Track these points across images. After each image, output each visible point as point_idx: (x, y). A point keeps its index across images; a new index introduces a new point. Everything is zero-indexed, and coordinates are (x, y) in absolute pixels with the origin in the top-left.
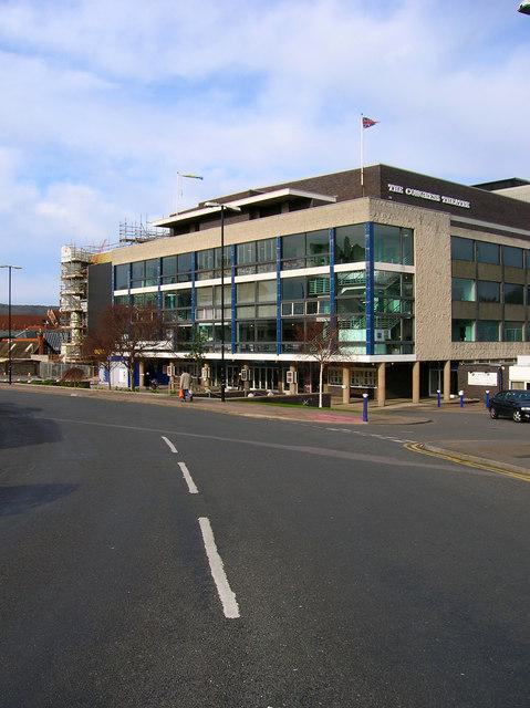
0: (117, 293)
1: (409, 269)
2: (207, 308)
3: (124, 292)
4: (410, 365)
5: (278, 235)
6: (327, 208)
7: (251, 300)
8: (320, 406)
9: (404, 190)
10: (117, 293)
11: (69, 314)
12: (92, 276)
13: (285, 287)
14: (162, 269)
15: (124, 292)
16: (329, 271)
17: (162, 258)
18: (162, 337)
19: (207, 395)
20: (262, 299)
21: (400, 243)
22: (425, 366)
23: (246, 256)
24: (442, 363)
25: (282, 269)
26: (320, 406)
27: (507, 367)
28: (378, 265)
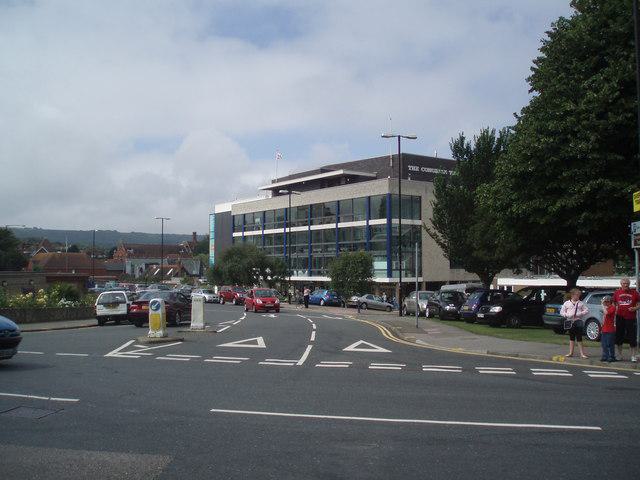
0: (235, 234)
1: (418, 222)
10: (235, 234)
15: (240, 234)
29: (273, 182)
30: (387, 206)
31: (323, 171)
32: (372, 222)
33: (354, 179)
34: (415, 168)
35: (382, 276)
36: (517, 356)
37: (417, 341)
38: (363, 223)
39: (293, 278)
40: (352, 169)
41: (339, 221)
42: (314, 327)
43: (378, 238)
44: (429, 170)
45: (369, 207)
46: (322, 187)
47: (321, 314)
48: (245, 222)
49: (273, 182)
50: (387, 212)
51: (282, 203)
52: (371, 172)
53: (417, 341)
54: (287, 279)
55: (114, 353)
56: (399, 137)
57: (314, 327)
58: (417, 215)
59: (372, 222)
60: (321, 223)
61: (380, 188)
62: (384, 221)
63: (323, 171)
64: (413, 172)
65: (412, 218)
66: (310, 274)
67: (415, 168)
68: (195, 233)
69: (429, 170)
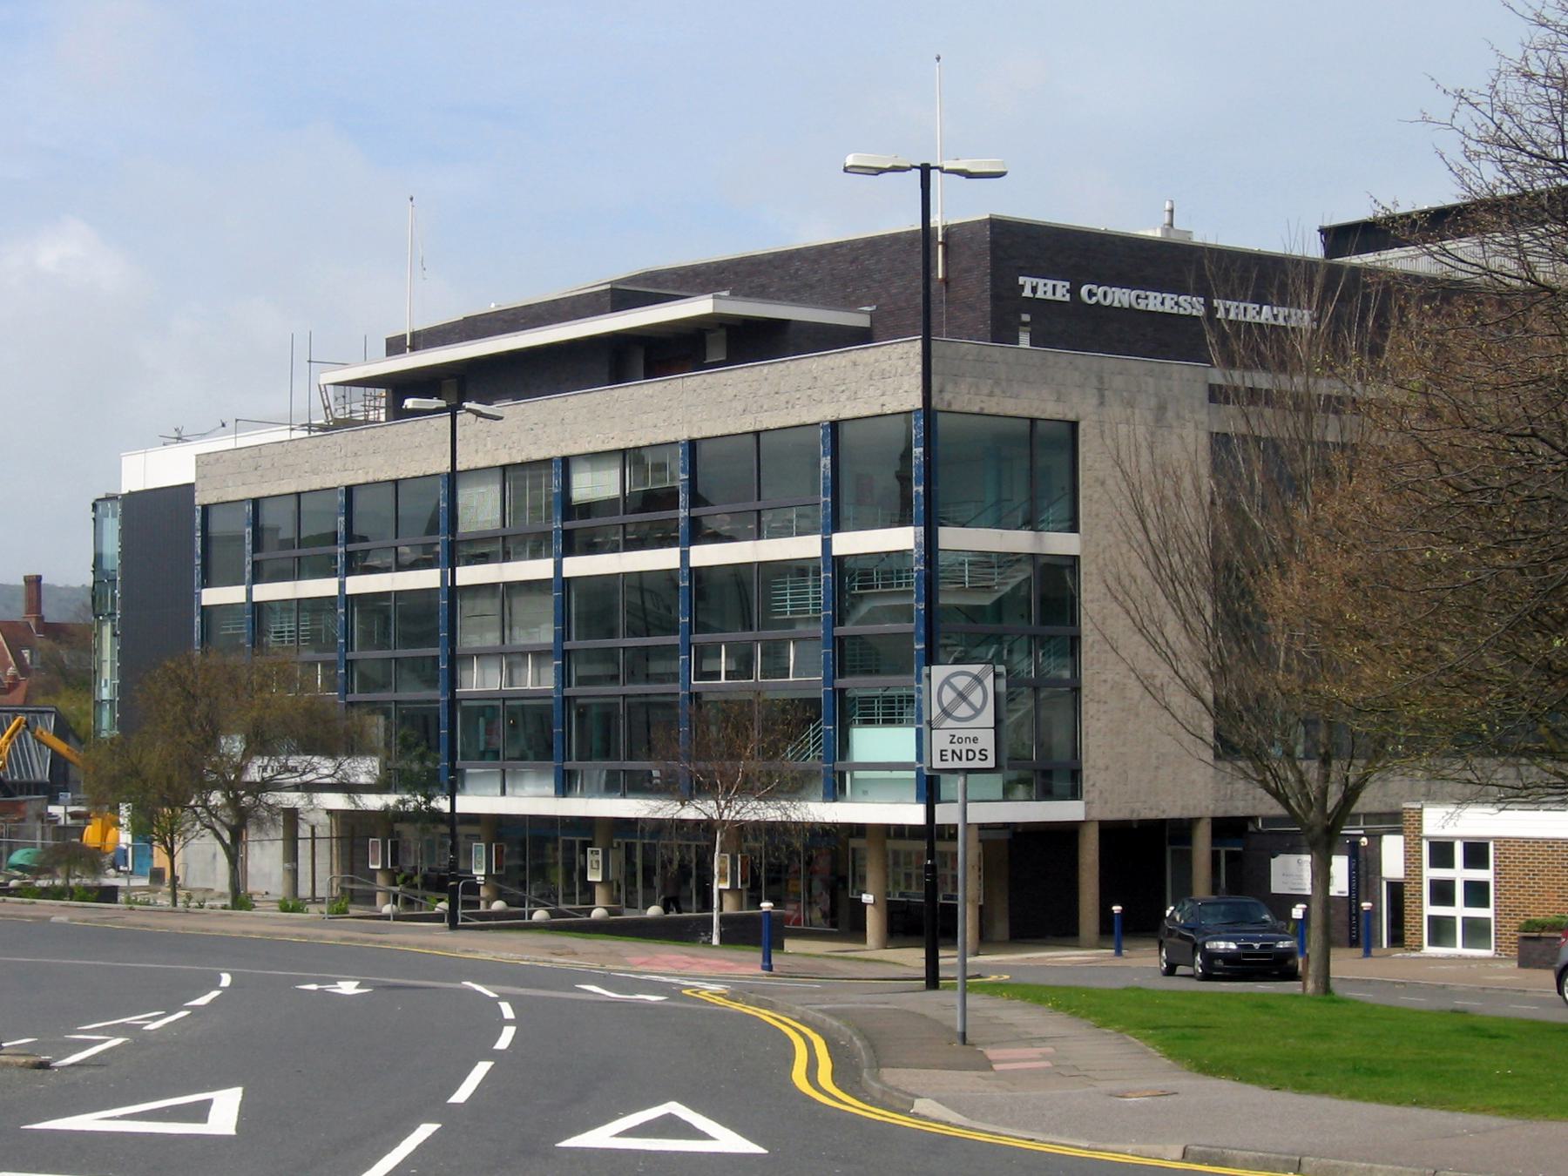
0: (212, 596)
1: (1060, 543)
2: (484, 655)
3: (233, 595)
4: (1067, 833)
5: (683, 434)
6: (365, 433)
7: (491, 639)
8: (715, 941)
9: (1074, 291)
10: (212, 596)
11: (1307, 757)
12: (163, 537)
13: (586, 606)
14: (344, 528)
15: (233, 595)
16: (550, 574)
17: (349, 490)
18: (353, 746)
19: (387, 917)
20: (521, 638)
21: (1039, 469)
22: (1115, 834)
23: (481, 509)
24: (1181, 830)
25: (836, 528)
26: (715, 941)
27: (1376, 839)
28: (950, 538)
29: (395, 346)
30: (932, 468)
31: (622, 296)
32: (848, 543)
33: (752, 341)
34: (1052, 289)
35: (887, 790)
36: (1340, 1158)
37: (920, 1106)
38: (806, 547)
39: (471, 802)
40: (761, 293)
41: (836, 524)
42: (507, 1011)
43: (871, 617)
44: (1121, 297)
45: (837, 467)
46: (618, 375)
47: (570, 979)
48: (279, 534)
49: (395, 346)
50: (918, 507)
51: (415, 449)
52: (850, 304)
53: (920, 1106)
54: (443, 804)
55: (727, 1141)
56: (925, 170)
57: (507, 1011)
58: (1060, 510)
59: (848, 543)
60: (630, 546)
61: (876, 383)
62: (903, 538)
63: (421, 340)
64: (1040, 307)
65: (1031, 522)
66: (565, 787)
67: (1052, 289)
68: (34, 583)
69: (1121, 297)
